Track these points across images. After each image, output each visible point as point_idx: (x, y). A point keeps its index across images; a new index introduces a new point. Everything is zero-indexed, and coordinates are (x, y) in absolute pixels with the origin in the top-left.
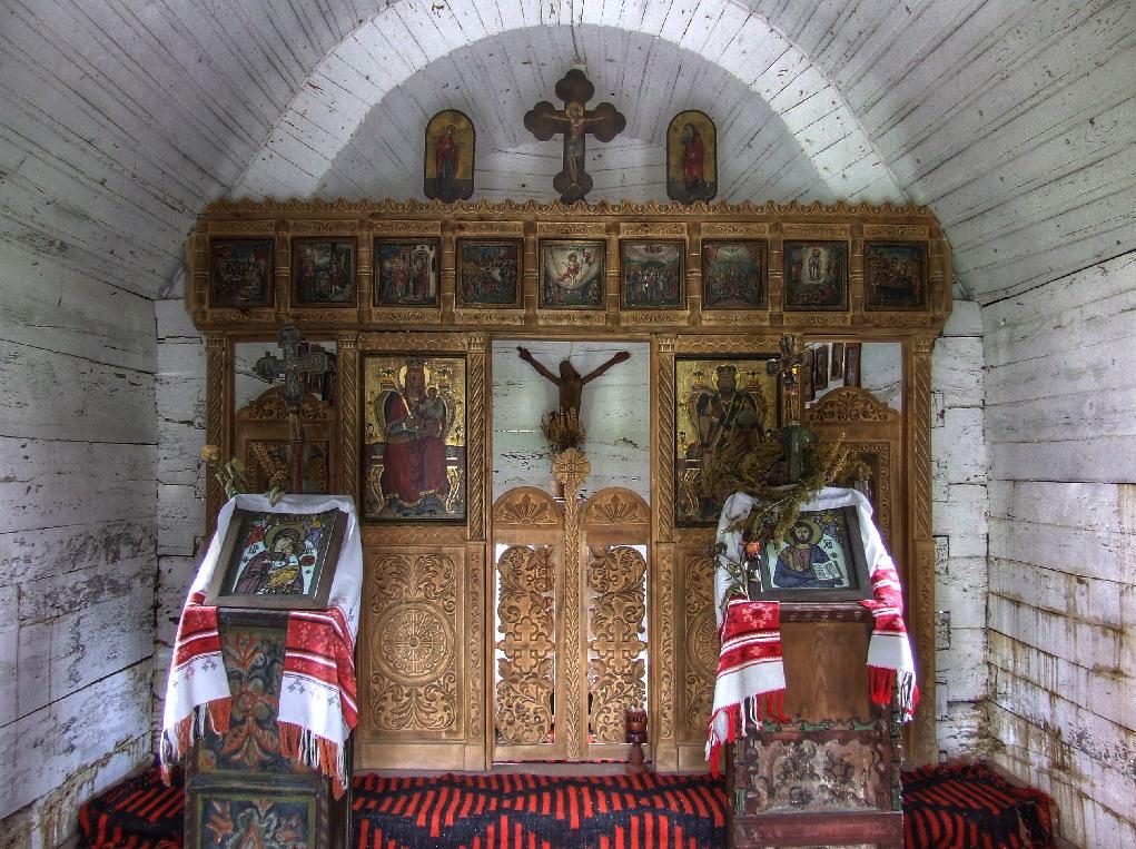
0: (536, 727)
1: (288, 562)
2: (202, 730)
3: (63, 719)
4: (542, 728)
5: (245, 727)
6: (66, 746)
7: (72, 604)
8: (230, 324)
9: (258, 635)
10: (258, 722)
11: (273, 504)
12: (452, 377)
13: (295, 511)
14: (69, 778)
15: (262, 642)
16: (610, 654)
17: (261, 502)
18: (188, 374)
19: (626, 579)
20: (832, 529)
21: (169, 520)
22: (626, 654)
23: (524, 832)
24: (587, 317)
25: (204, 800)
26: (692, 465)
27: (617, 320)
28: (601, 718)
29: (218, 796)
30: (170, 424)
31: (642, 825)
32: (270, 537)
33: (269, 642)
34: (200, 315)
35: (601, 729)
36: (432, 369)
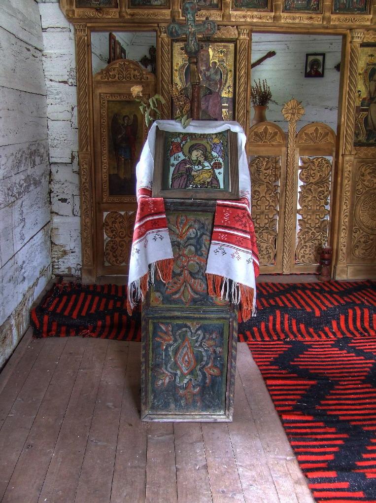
0: (266, 256)
1: (204, 167)
2: (153, 280)
3: (20, 263)
4: (270, 257)
5: (182, 278)
6: (21, 278)
7: (19, 193)
8: (90, 19)
9: (192, 217)
10: (191, 273)
11: (184, 128)
12: (226, 55)
13: (199, 131)
14: (24, 295)
15: (195, 222)
16: (309, 217)
17: (175, 126)
18: (62, 51)
19: (320, 175)
20: (218, 148)
21: (55, 141)
22: (318, 217)
23: (289, 319)
24: (311, 18)
25: (154, 323)
26: (364, 110)
27: (329, 20)
28: (302, 251)
29: (164, 321)
30: (53, 83)
31: (355, 314)
32: (186, 149)
33: (199, 221)
34: (71, 13)
35: (302, 257)
36: (214, 50)
